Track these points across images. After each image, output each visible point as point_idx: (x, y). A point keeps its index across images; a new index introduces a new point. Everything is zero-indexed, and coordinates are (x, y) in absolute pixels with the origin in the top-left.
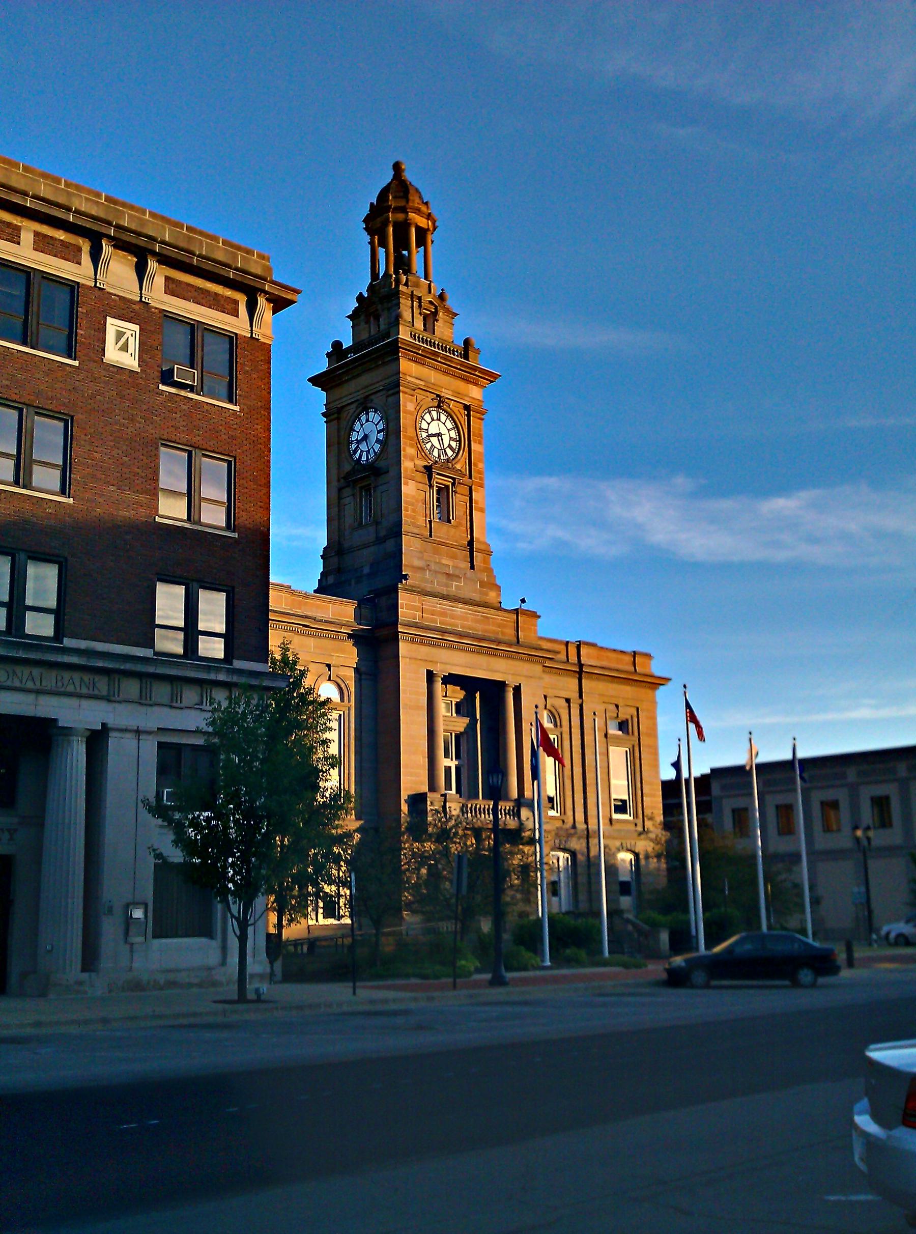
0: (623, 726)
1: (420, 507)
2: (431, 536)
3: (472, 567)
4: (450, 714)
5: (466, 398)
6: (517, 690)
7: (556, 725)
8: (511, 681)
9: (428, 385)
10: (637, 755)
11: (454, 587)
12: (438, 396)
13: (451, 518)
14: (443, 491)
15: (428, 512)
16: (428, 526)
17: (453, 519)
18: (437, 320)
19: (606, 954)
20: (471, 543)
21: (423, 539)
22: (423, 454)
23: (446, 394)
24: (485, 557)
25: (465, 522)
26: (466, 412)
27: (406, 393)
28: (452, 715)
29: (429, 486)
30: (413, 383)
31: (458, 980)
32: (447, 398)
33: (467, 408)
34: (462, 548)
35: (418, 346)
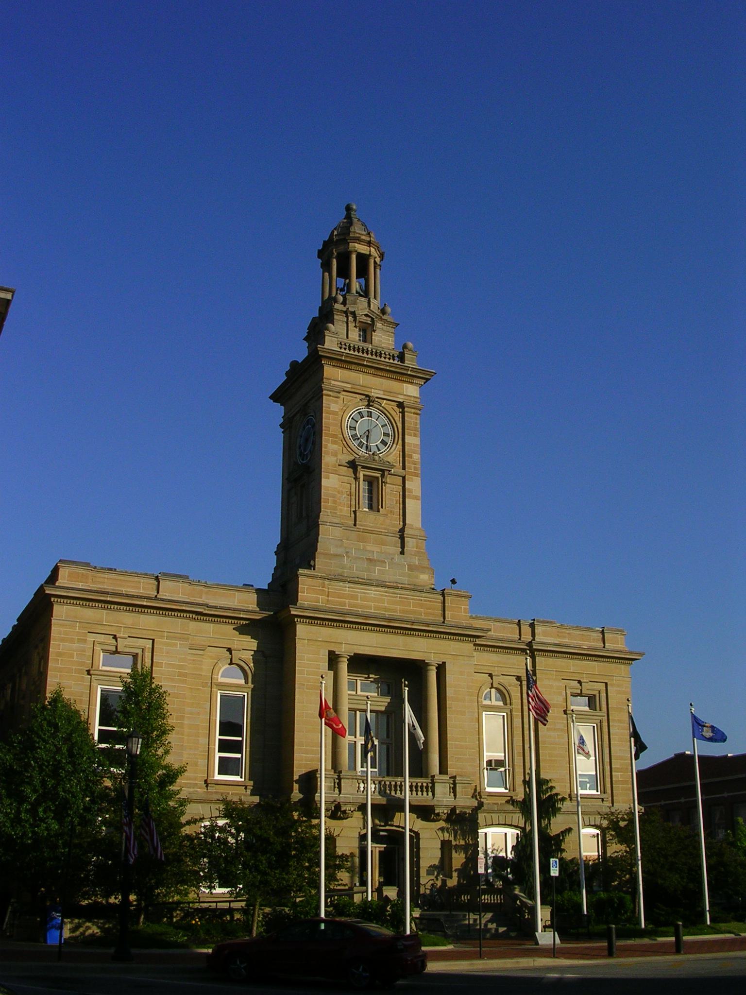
0: (592, 702)
1: (344, 499)
2: (355, 525)
3: (402, 553)
4: (354, 693)
5: (399, 396)
6: (441, 669)
7: (505, 704)
8: (433, 660)
9: (354, 386)
10: (605, 729)
11: (377, 573)
12: (367, 396)
13: (380, 507)
14: (371, 482)
15: (353, 503)
16: (353, 515)
17: (382, 507)
18: (374, 331)
19: (708, 923)
20: (402, 531)
21: (346, 528)
22: (349, 449)
23: (374, 393)
24: (417, 542)
25: (397, 509)
26: (401, 410)
27: (329, 396)
28: (356, 693)
29: (354, 478)
30: (337, 386)
31: (483, 949)
32: (377, 398)
33: (401, 405)
34: (392, 535)
35: (341, 353)
